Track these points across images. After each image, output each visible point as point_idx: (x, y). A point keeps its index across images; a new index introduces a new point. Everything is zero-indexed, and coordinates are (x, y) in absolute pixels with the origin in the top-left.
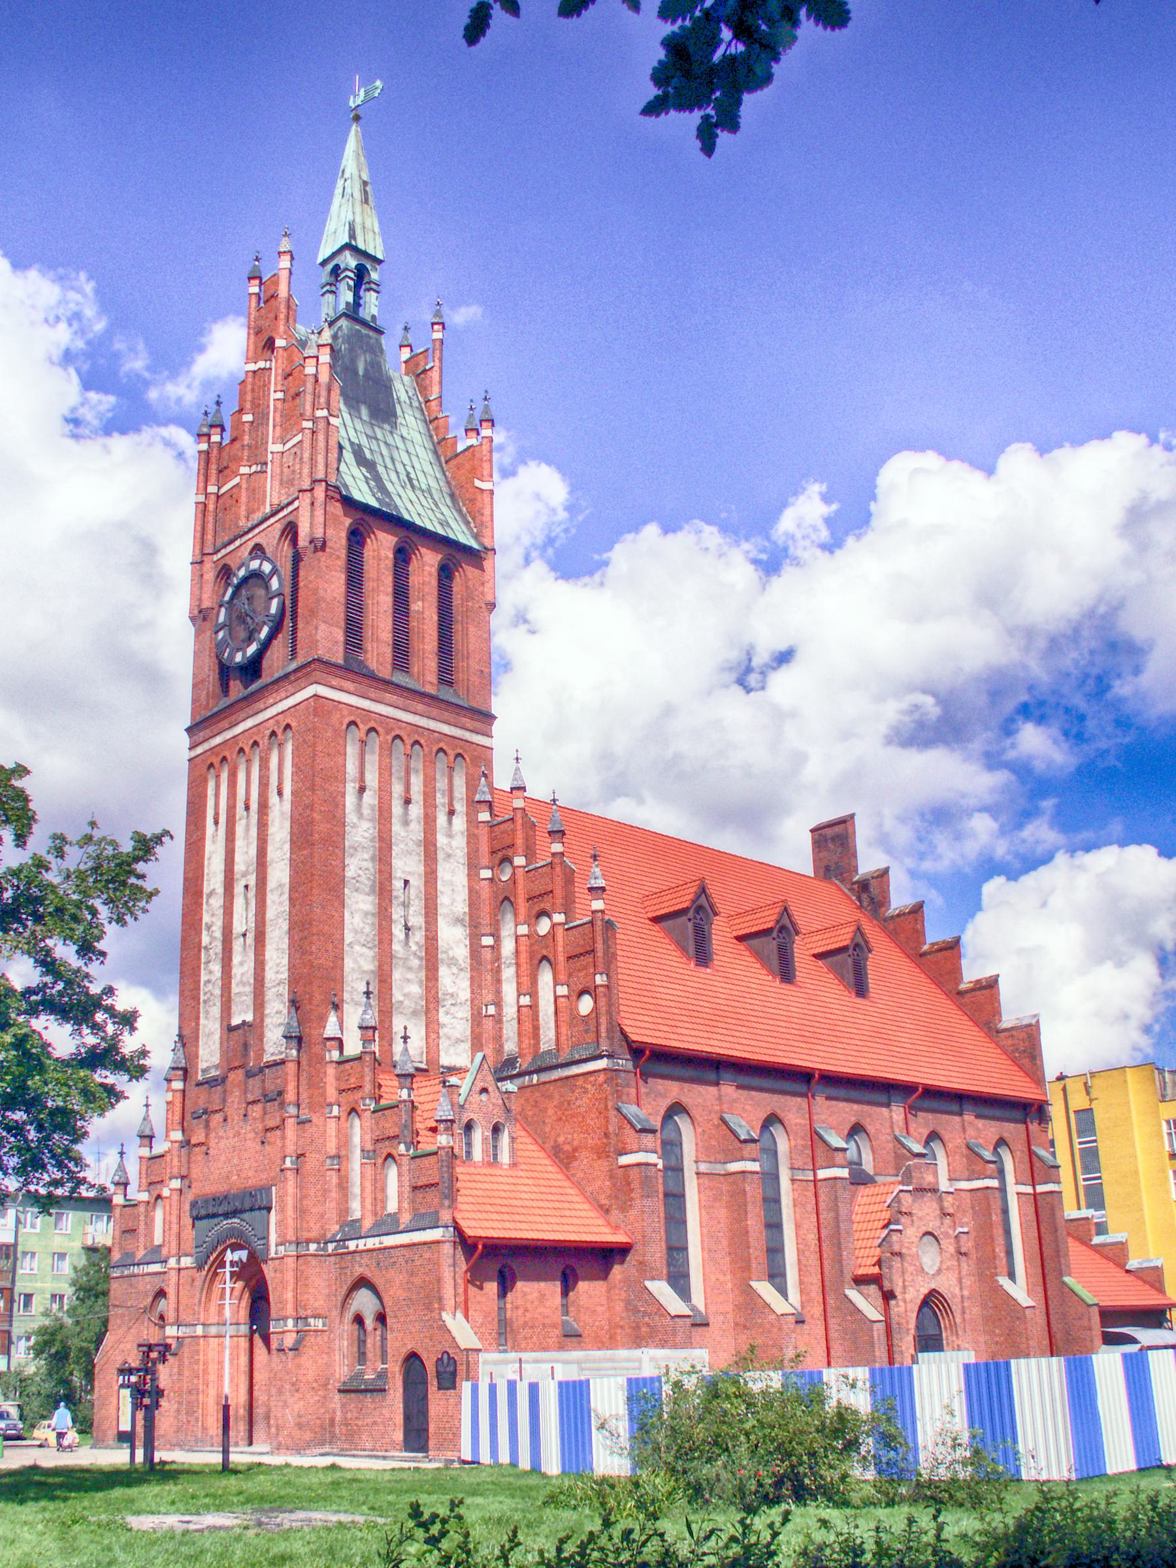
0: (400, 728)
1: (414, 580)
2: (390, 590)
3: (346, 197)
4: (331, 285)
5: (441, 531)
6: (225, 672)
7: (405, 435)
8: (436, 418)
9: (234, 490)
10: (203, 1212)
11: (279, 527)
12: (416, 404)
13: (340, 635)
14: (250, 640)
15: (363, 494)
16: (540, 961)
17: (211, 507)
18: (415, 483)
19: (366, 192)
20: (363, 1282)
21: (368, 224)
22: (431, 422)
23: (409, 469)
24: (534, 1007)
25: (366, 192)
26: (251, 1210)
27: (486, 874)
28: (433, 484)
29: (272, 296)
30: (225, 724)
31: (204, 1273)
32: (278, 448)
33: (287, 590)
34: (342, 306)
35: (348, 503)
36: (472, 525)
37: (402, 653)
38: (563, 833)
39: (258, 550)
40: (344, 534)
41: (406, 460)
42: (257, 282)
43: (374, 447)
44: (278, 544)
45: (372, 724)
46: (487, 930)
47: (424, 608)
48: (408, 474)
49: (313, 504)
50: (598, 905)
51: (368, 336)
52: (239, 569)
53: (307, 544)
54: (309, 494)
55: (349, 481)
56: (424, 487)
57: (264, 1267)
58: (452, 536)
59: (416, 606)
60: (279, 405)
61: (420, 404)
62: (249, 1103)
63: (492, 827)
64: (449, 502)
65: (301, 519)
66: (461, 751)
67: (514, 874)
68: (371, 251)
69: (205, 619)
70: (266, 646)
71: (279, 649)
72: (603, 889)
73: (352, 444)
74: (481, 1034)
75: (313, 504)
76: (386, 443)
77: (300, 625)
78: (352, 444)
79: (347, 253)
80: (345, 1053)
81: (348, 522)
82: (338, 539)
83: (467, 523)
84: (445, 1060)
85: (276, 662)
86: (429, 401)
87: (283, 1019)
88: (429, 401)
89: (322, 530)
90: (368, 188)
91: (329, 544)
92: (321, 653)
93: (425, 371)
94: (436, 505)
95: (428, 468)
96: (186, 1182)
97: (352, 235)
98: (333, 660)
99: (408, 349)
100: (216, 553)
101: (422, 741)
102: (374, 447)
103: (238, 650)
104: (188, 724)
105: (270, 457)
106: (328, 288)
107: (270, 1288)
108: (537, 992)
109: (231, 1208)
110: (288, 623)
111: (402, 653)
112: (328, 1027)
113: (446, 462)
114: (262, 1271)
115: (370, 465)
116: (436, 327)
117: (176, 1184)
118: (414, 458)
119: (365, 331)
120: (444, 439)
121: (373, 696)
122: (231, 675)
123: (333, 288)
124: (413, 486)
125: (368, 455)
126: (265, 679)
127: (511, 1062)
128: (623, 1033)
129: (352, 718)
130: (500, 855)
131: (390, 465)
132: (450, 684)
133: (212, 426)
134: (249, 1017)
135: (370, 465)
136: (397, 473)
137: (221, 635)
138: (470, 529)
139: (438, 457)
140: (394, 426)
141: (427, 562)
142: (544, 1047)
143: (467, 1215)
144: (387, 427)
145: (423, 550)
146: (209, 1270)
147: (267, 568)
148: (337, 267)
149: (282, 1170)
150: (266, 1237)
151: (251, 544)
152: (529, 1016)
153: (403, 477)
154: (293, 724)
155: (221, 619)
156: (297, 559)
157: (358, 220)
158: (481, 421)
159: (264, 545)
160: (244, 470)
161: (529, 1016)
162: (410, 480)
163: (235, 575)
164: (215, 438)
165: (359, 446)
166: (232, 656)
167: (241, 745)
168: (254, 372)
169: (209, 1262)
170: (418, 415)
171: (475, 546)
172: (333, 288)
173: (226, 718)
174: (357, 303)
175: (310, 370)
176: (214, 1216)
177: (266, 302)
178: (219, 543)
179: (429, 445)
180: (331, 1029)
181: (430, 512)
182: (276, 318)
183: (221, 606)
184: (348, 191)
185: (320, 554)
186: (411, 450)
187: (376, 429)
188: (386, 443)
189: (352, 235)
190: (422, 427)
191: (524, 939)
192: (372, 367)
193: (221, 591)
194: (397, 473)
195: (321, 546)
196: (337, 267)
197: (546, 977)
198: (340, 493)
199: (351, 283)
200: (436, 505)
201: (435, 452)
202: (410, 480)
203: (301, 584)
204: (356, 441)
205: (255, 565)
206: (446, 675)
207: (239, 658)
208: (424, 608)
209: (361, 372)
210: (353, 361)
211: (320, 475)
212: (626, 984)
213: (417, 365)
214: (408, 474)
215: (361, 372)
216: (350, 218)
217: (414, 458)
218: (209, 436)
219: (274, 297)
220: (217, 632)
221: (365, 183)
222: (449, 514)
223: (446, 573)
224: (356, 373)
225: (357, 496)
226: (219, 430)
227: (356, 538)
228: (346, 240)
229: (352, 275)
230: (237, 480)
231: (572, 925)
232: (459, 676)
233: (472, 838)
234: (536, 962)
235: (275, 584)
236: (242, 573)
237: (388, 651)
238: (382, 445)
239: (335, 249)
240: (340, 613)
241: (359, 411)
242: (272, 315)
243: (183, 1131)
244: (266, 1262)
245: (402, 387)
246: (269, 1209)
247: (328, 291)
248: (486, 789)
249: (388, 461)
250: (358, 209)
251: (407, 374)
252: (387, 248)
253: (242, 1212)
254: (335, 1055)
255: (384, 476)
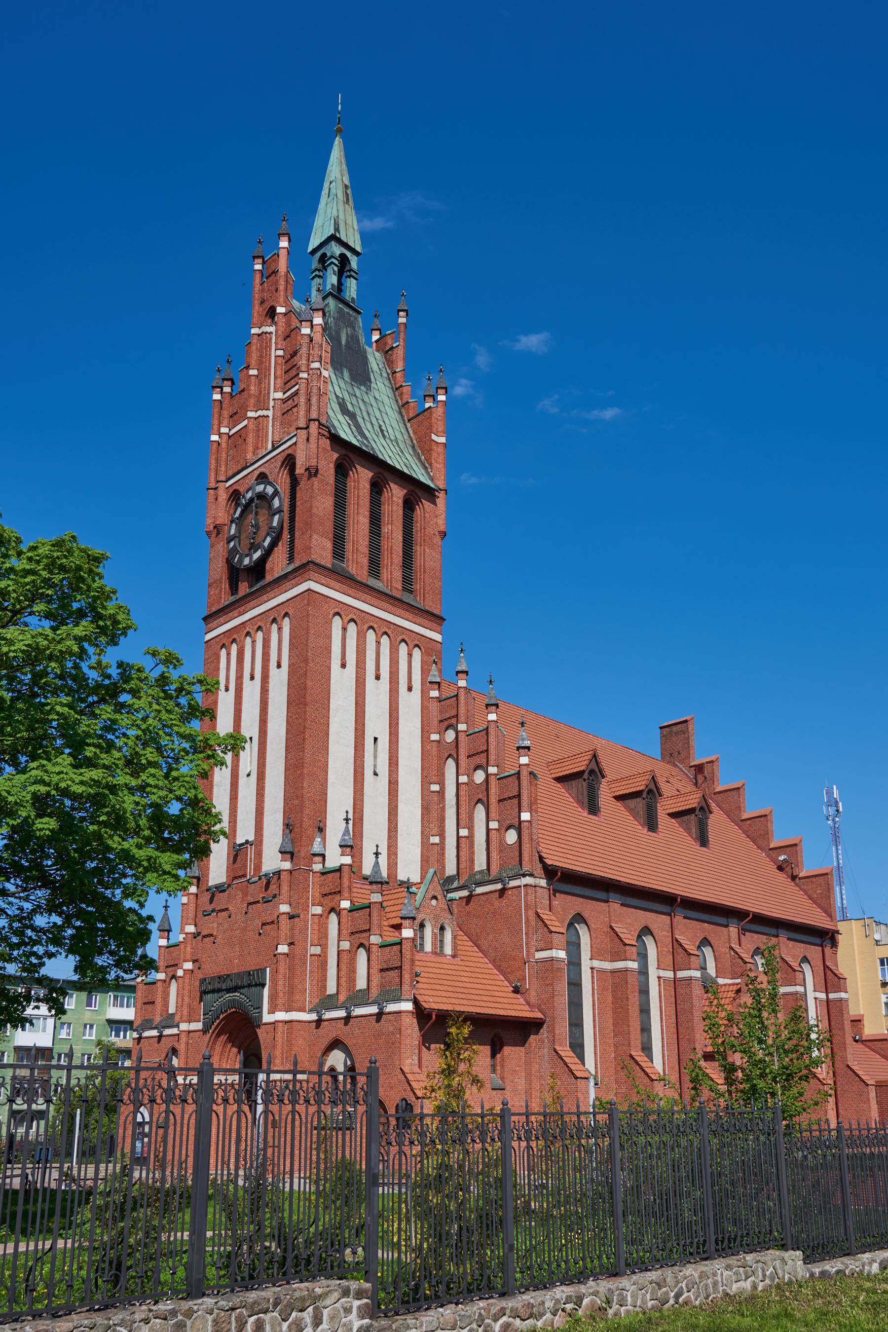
0: (372, 621)
1: (385, 509)
2: (367, 513)
3: (332, 196)
4: (319, 270)
5: (406, 471)
6: (234, 574)
7: (377, 397)
8: (401, 386)
9: (242, 431)
10: (210, 987)
11: (281, 458)
12: (385, 375)
13: (329, 545)
14: (254, 547)
15: (346, 433)
16: (476, 803)
17: (224, 445)
18: (386, 433)
19: (347, 195)
20: (336, 1044)
21: (349, 221)
22: (397, 389)
23: (382, 423)
24: (470, 838)
25: (347, 195)
26: (249, 986)
27: (435, 737)
28: (399, 436)
29: (273, 272)
30: (235, 613)
31: (208, 1035)
32: (279, 395)
33: (286, 508)
34: (329, 287)
35: (336, 440)
36: (429, 470)
37: (375, 566)
38: (497, 706)
39: (262, 478)
40: (332, 466)
41: (379, 416)
42: (260, 261)
43: (354, 402)
44: (279, 472)
45: (352, 616)
46: (435, 779)
47: (393, 531)
48: (380, 427)
49: (308, 440)
50: (524, 760)
51: (348, 313)
52: (247, 492)
53: (302, 471)
54: (304, 432)
55: (336, 424)
56: (393, 438)
57: (258, 1030)
58: (414, 476)
59: (385, 529)
60: (280, 360)
61: (388, 375)
62: (249, 904)
63: (439, 700)
64: (411, 452)
65: (298, 451)
66: (418, 643)
67: (457, 738)
68: (351, 244)
69: (218, 533)
70: (269, 552)
71: (280, 554)
72: (528, 748)
73: (337, 397)
74: (428, 857)
75: (308, 440)
76: (363, 400)
77: (297, 534)
78: (337, 397)
79: (333, 243)
80: (327, 865)
81: (336, 456)
82: (328, 471)
83: (425, 468)
84: (402, 876)
85: (278, 564)
86: (395, 372)
87: (279, 840)
88: (395, 372)
89: (315, 460)
90: (349, 191)
91: (320, 472)
92: (314, 557)
93: (392, 348)
94: (402, 452)
95: (395, 424)
96: (197, 964)
97: (337, 229)
98: (323, 563)
99: (378, 332)
100: (226, 481)
101: (389, 632)
102: (354, 402)
103: (247, 555)
104: (205, 614)
105: (272, 403)
106: (317, 273)
107: (262, 1047)
108: (473, 827)
109: (234, 984)
110: (286, 536)
111: (375, 566)
112: (315, 846)
113: (409, 421)
114: (256, 1034)
115: (352, 416)
116: (401, 314)
117: (188, 966)
118: (384, 415)
119: (346, 310)
120: (408, 402)
121: (353, 594)
122: (240, 578)
123: (321, 274)
124: (384, 436)
125: (350, 408)
126: (269, 578)
127: (450, 879)
128: (541, 859)
129: (336, 610)
130: (446, 723)
131: (366, 418)
132: (411, 592)
133: (224, 380)
134: (251, 838)
135: (352, 416)
136: (372, 424)
137: (232, 544)
138: (428, 474)
139: (402, 417)
140: (369, 388)
141: (396, 494)
142: (477, 868)
143: (422, 992)
144: (362, 388)
145: (392, 485)
146: (213, 1032)
147: (270, 490)
148: (324, 255)
149: (275, 955)
150: (260, 1007)
151: (257, 473)
152: (464, 845)
153: (377, 428)
154: (290, 613)
155: (233, 532)
156: (294, 482)
157: (341, 216)
158: (437, 388)
159: (268, 473)
160: (250, 414)
161: (464, 845)
162: (382, 431)
163: (244, 497)
164: (227, 389)
165: (343, 399)
166: (241, 560)
167: (248, 629)
168: (259, 335)
169: (213, 1027)
170: (387, 383)
171: (432, 485)
172: (321, 274)
173: (236, 609)
174: (340, 287)
175: (306, 331)
176: (219, 990)
177: (267, 278)
178: (230, 473)
179: (395, 407)
180: (316, 848)
181: (397, 457)
182: (277, 290)
183: (232, 522)
184: (333, 191)
185: (314, 478)
186: (382, 409)
187: (355, 389)
188: (363, 400)
189: (337, 229)
190: (390, 393)
191: (463, 786)
192: (352, 339)
193: (232, 511)
194: (372, 424)
195: (313, 472)
196: (324, 255)
197: (480, 812)
198: (329, 432)
199: (336, 269)
200: (402, 452)
201: (400, 413)
202: (382, 431)
203: (298, 503)
204: (341, 396)
205: (260, 488)
206: (408, 581)
207: (246, 561)
208: (393, 531)
209: (344, 342)
210: (338, 333)
211: (314, 415)
212: (542, 807)
213: (386, 344)
214: (380, 427)
215: (344, 342)
216: (335, 213)
217: (384, 415)
218: (222, 388)
219: (275, 272)
220: (228, 542)
221: (346, 187)
222: (413, 462)
223: (409, 505)
224: (341, 342)
225: (343, 435)
226: (229, 383)
227: (342, 470)
228: (332, 231)
229: (336, 262)
230: (245, 422)
231: (502, 776)
232: (417, 586)
233: (424, 709)
234: (473, 804)
235: (276, 503)
236: (249, 495)
237: (365, 561)
238: (360, 402)
239: (323, 239)
240: (329, 525)
241: (342, 373)
242: (273, 288)
243: (196, 926)
244: (259, 1026)
245: (375, 360)
246: (263, 985)
247: (316, 276)
248: (436, 673)
249: (365, 414)
250: (341, 207)
251: (378, 350)
252: (363, 244)
253: (242, 987)
254: (318, 867)
255: (362, 425)
